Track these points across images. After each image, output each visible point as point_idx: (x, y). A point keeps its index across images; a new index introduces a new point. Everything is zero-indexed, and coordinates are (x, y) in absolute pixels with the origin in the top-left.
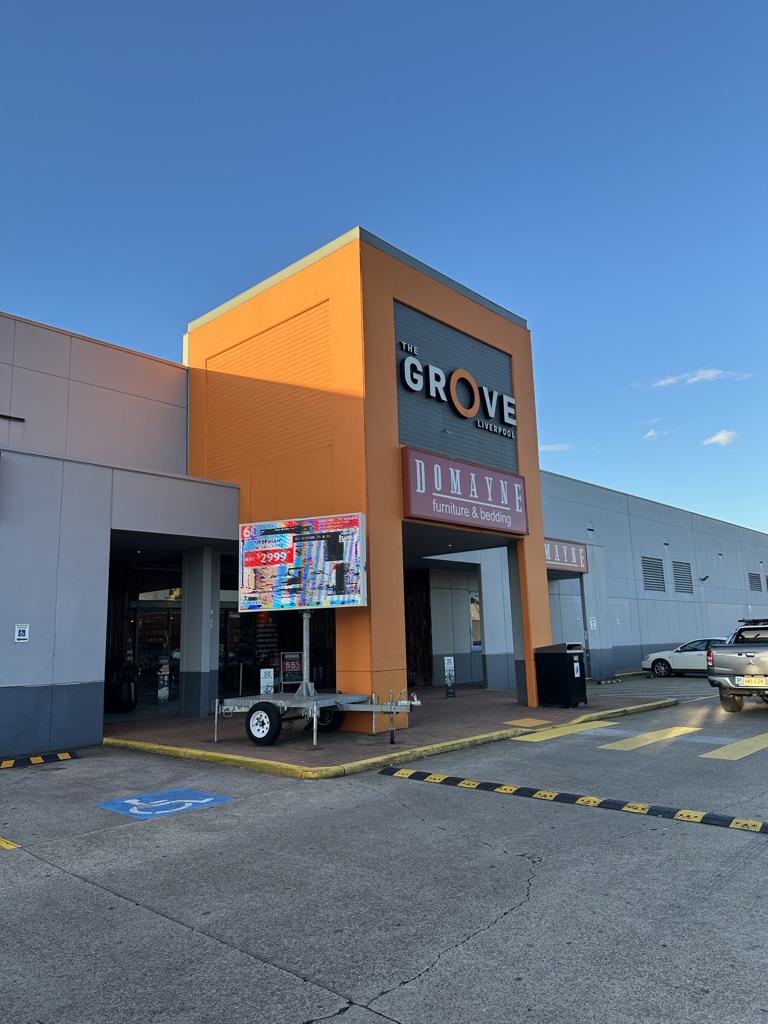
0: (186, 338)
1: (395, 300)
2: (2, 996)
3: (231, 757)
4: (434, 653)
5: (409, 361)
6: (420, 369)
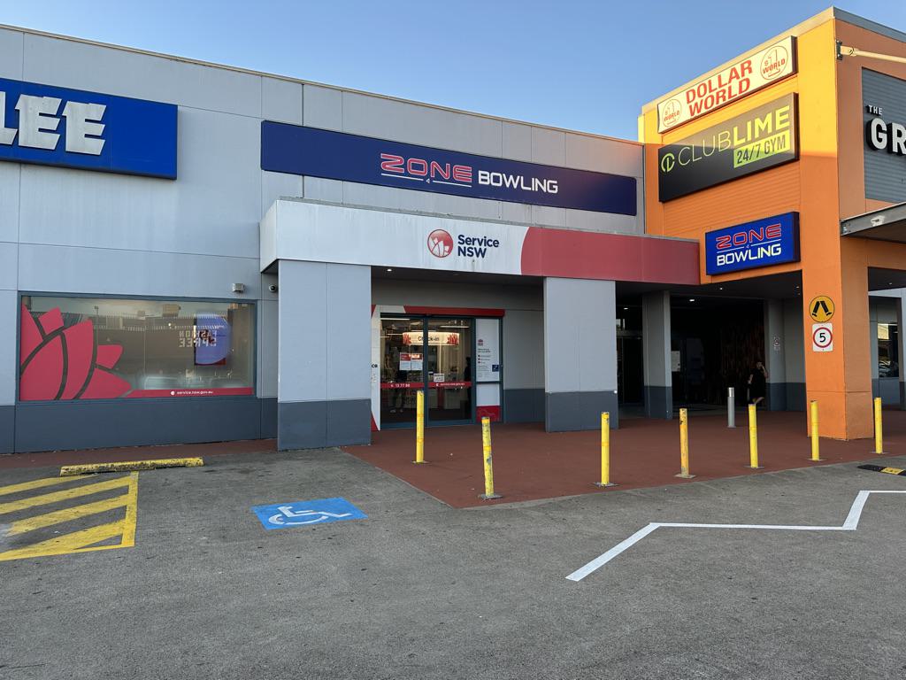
0: (641, 120)
1: (863, 68)
2: (905, 621)
6: (885, 128)
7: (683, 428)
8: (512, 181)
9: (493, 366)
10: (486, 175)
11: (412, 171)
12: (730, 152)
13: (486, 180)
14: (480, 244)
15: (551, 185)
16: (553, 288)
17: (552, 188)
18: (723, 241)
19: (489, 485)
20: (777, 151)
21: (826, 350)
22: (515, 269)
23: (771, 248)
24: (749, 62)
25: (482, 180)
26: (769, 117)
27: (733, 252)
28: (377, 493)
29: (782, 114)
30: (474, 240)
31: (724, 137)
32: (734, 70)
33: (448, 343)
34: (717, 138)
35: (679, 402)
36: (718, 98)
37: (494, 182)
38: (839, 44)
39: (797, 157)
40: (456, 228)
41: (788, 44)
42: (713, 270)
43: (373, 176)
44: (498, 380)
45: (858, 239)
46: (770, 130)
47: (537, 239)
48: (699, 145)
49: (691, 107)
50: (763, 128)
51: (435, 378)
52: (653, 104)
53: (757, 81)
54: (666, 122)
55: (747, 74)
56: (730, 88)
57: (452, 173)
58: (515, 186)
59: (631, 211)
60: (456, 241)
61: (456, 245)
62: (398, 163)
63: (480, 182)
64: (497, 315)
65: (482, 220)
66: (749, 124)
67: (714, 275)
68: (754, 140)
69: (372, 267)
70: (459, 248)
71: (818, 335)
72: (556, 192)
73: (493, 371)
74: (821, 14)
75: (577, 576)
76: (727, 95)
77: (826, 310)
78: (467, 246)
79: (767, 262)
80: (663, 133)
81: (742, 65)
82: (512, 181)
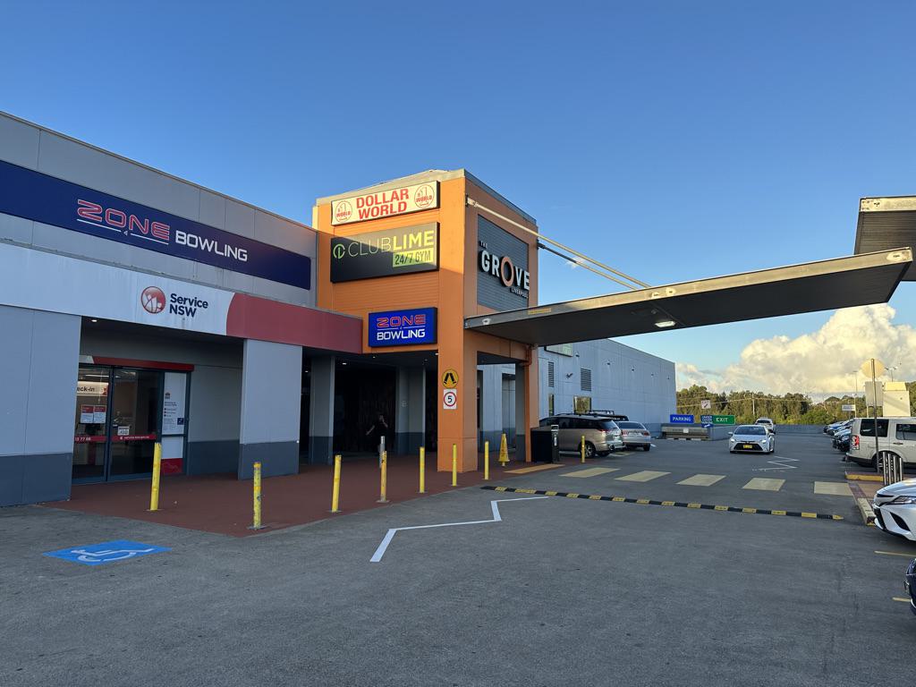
0: (315, 210)
3: (455, 461)
4: (224, 333)
5: (485, 253)
7: (383, 466)
8: (207, 245)
9: (179, 419)
10: (183, 236)
11: (110, 221)
12: (390, 254)
13: (183, 241)
14: (191, 304)
15: (242, 253)
16: (253, 350)
17: (242, 256)
18: (383, 322)
19: (257, 518)
20: (424, 261)
21: (452, 408)
22: (220, 329)
23: (418, 332)
24: (407, 191)
25: (179, 239)
26: (420, 235)
27: (390, 331)
28: (151, 535)
29: (429, 235)
30: (186, 299)
31: (385, 242)
32: (395, 192)
33: (104, 394)
34: (380, 242)
35: (336, 451)
36: (382, 210)
37: (195, 239)
38: (467, 196)
39: (437, 269)
40: (169, 287)
41: (434, 185)
42: (373, 342)
43: (69, 221)
44: (183, 433)
45: (474, 332)
46: (420, 245)
47: (241, 306)
48: (366, 243)
49: (360, 211)
50: (415, 242)
51: (119, 431)
52: (327, 200)
53: (412, 206)
54: (339, 218)
55: (405, 199)
56: (392, 205)
57: (150, 229)
58: (210, 249)
59: (306, 285)
60: (168, 299)
61: (168, 303)
62: (95, 211)
63: (177, 241)
64: (186, 369)
65: (194, 282)
66: (405, 236)
67: (373, 347)
68: (408, 249)
69: (84, 318)
70: (171, 306)
71: (447, 398)
72: (245, 260)
73: (178, 424)
74: (457, 171)
75: (377, 557)
76: (389, 209)
77: (453, 380)
78: (179, 305)
79: (414, 341)
80: (335, 226)
81: (402, 191)
82: (207, 245)
